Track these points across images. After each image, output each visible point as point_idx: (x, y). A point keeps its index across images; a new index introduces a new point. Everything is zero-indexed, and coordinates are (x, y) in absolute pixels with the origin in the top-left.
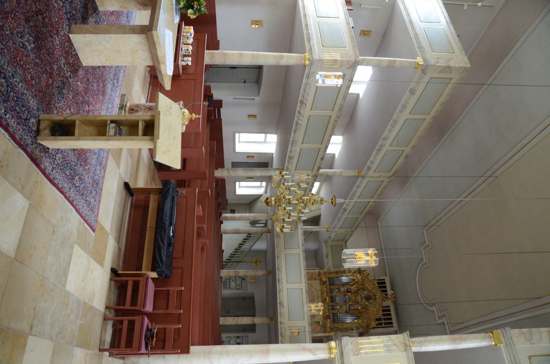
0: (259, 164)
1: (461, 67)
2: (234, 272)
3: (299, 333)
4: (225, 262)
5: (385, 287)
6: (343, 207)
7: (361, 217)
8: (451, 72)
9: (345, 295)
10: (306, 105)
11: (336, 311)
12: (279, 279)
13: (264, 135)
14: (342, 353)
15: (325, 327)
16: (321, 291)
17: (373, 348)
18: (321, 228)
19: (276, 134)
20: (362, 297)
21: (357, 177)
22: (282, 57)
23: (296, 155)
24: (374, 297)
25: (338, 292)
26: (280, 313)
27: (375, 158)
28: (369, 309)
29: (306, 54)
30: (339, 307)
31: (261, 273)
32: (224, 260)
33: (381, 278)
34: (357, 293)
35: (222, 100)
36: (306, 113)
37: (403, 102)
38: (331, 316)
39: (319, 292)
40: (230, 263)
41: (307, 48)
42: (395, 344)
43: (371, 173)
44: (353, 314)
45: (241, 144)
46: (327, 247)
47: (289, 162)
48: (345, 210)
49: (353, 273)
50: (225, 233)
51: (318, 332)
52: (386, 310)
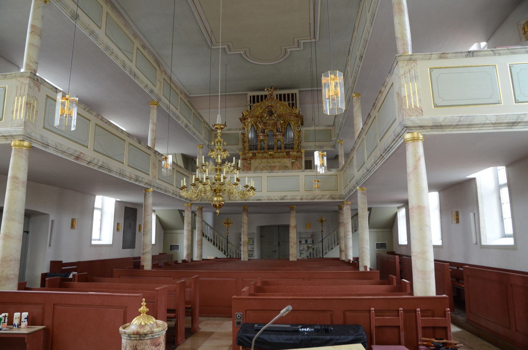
0: (129, 218)
2: (244, 246)
4: (227, 255)
5: (262, 96)
6: (184, 127)
7: (193, 111)
9: (268, 135)
10: (82, 153)
11: (283, 146)
12: (257, 200)
13: (95, 211)
14: (421, 127)
15: (297, 157)
19: (95, 196)
20: (269, 119)
21: (158, 106)
22: (15, 178)
23: (135, 173)
24: (270, 107)
26: (291, 199)
28: (281, 113)
29: (12, 144)
30: (279, 143)
31: (245, 218)
35: (51, 262)
36: (90, 155)
38: (287, 150)
39: (263, 160)
40: (229, 252)
43: (156, 90)
44: (286, 130)
45: (103, 237)
47: (140, 182)
48: (187, 126)
49: (245, 125)
50: (201, 256)
51: (301, 164)
52: (281, 97)
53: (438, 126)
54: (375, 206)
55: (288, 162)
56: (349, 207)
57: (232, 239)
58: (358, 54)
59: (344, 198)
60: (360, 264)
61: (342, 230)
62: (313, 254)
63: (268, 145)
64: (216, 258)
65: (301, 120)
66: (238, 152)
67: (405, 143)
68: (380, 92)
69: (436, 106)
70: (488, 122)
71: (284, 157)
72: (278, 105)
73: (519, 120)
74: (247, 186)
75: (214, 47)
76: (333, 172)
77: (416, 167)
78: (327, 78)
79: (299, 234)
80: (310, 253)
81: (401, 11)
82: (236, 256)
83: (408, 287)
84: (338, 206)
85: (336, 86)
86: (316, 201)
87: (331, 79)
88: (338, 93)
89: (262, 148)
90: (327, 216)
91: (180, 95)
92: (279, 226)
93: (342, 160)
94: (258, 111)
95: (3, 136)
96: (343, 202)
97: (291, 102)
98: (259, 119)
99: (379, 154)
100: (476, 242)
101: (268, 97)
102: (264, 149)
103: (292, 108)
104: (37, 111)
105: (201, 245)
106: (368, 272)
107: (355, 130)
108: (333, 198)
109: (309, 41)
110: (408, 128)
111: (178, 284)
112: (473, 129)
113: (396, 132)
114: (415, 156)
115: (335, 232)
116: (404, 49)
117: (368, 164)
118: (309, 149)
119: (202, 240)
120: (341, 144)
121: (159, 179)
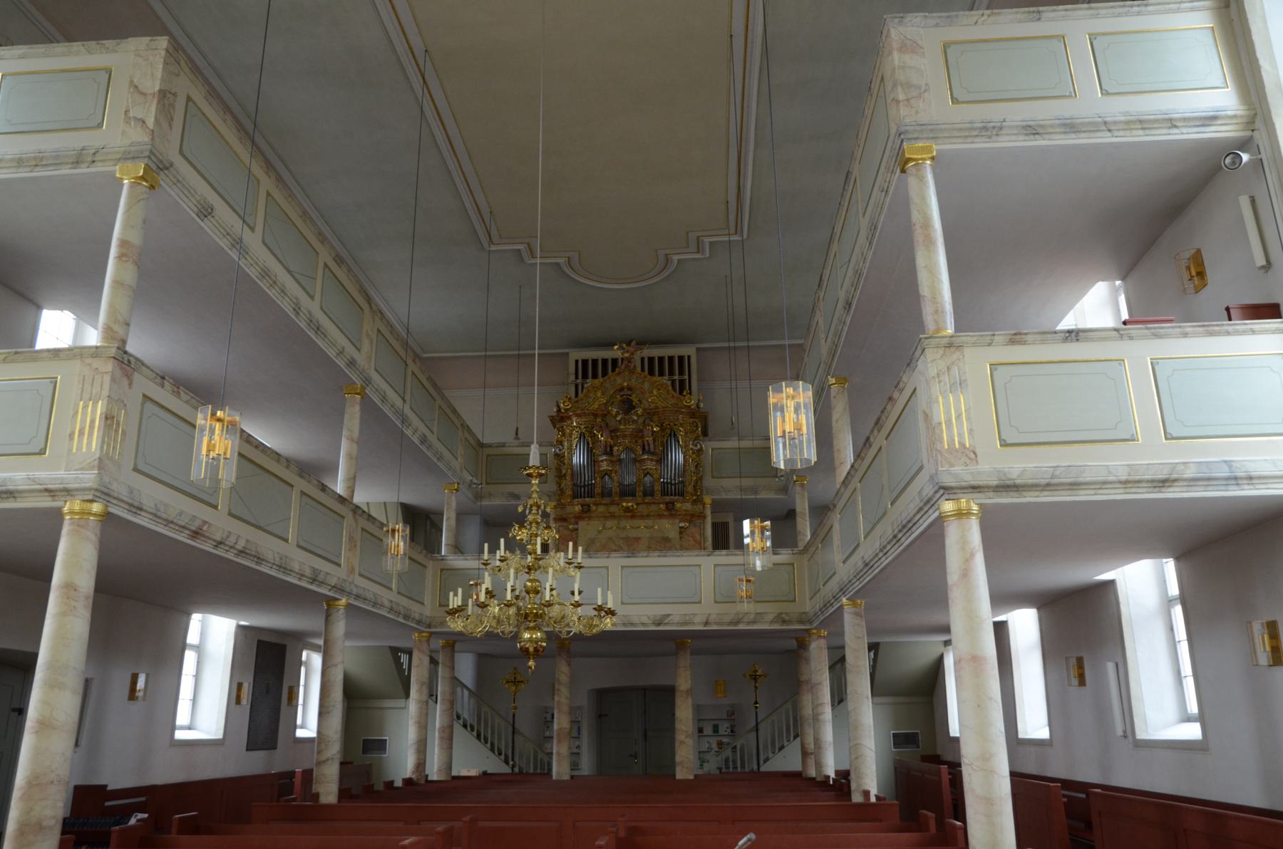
0: (265, 670)
1: (166, 63)
2: (559, 742)
3: (748, 581)
4: (513, 766)
5: (605, 361)
6: (417, 442)
8: (175, 95)
9: (620, 460)
10: (205, 522)
11: (657, 487)
15: (692, 515)
16: (606, 518)
17: (959, 416)
18: (447, 503)
19: (189, 615)
21: (365, 398)
22: (69, 587)
25: (610, 477)
27: (332, 344)
28: (653, 406)
29: (66, 509)
30: (648, 479)
31: (563, 670)
32: (509, 771)
33: (572, 369)
34: (615, 430)
37: (224, 243)
38: (668, 499)
39: (609, 523)
40: (517, 759)
41: (45, 503)
42: (949, 369)
43: (361, 359)
44: (666, 447)
46: (490, 495)
47: (322, 583)
48: (424, 440)
49: (563, 435)
50: (449, 767)
51: (703, 534)
52: (652, 366)
53: (1008, 486)
54: (887, 639)
55: (669, 527)
56: (823, 643)
57: (525, 724)
58: (842, 295)
59: (810, 622)
60: (853, 786)
61: (806, 700)
62: (734, 762)
63: (621, 484)
64: (485, 773)
65: (702, 424)
67: (941, 520)
68: (890, 399)
69: (1004, 444)
70: (1111, 478)
71: (661, 516)
72: (646, 386)
73: (1174, 476)
74: (599, 609)
75: (493, 248)
76: (784, 556)
77: (966, 574)
78: (779, 395)
79: (697, 709)
80: (727, 760)
81: (930, 241)
82: (535, 768)
83: (960, 833)
84: (797, 639)
85: (797, 410)
86: (741, 627)
87: (788, 397)
88: (801, 425)
89: (606, 493)
90: (768, 665)
91: (412, 367)
92: (644, 690)
93: (805, 528)
94: (597, 400)
95: (46, 490)
96: (807, 631)
97: (676, 377)
98: (599, 420)
99: (889, 534)
100: (1125, 732)
101: (621, 367)
102: (610, 494)
103: (681, 393)
104: (124, 432)
105: (448, 739)
106: (873, 804)
107: (837, 463)
108: (784, 622)
109: (726, 239)
110: (947, 491)
111: (438, 833)
112: (1082, 492)
113: (924, 493)
114: (963, 549)
115: (789, 705)
116: (936, 322)
117: (867, 550)
118: (724, 496)
119: (451, 727)
120: (802, 486)
121: (361, 575)
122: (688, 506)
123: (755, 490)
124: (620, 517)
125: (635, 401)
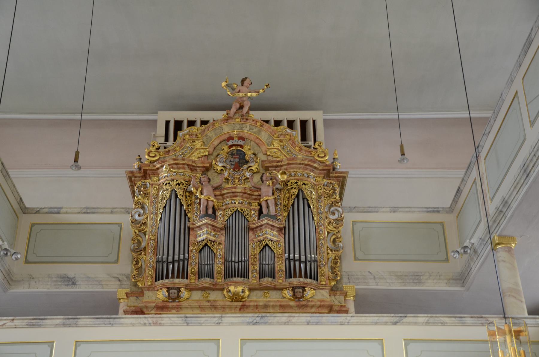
24: (236, 141)
38: (295, 281)
46: (31, 278)
66: (112, 287)
118: (372, 286)
120: (509, 250)
122: (324, 295)
123: (417, 278)
124: (224, 307)
125: (249, 154)
